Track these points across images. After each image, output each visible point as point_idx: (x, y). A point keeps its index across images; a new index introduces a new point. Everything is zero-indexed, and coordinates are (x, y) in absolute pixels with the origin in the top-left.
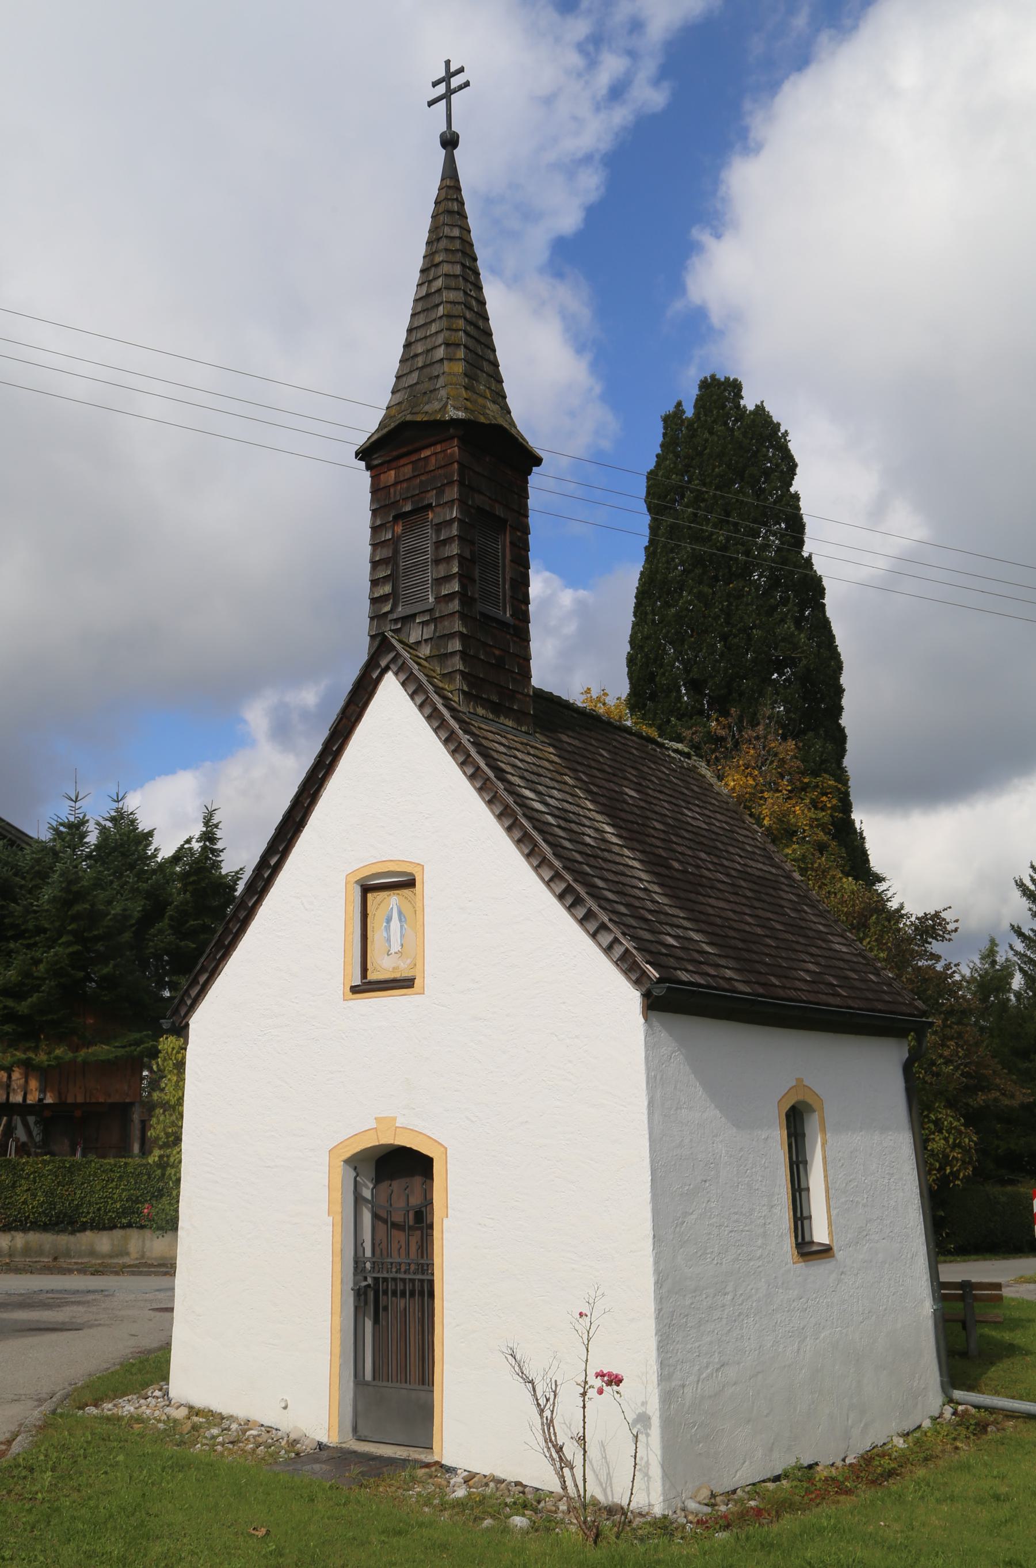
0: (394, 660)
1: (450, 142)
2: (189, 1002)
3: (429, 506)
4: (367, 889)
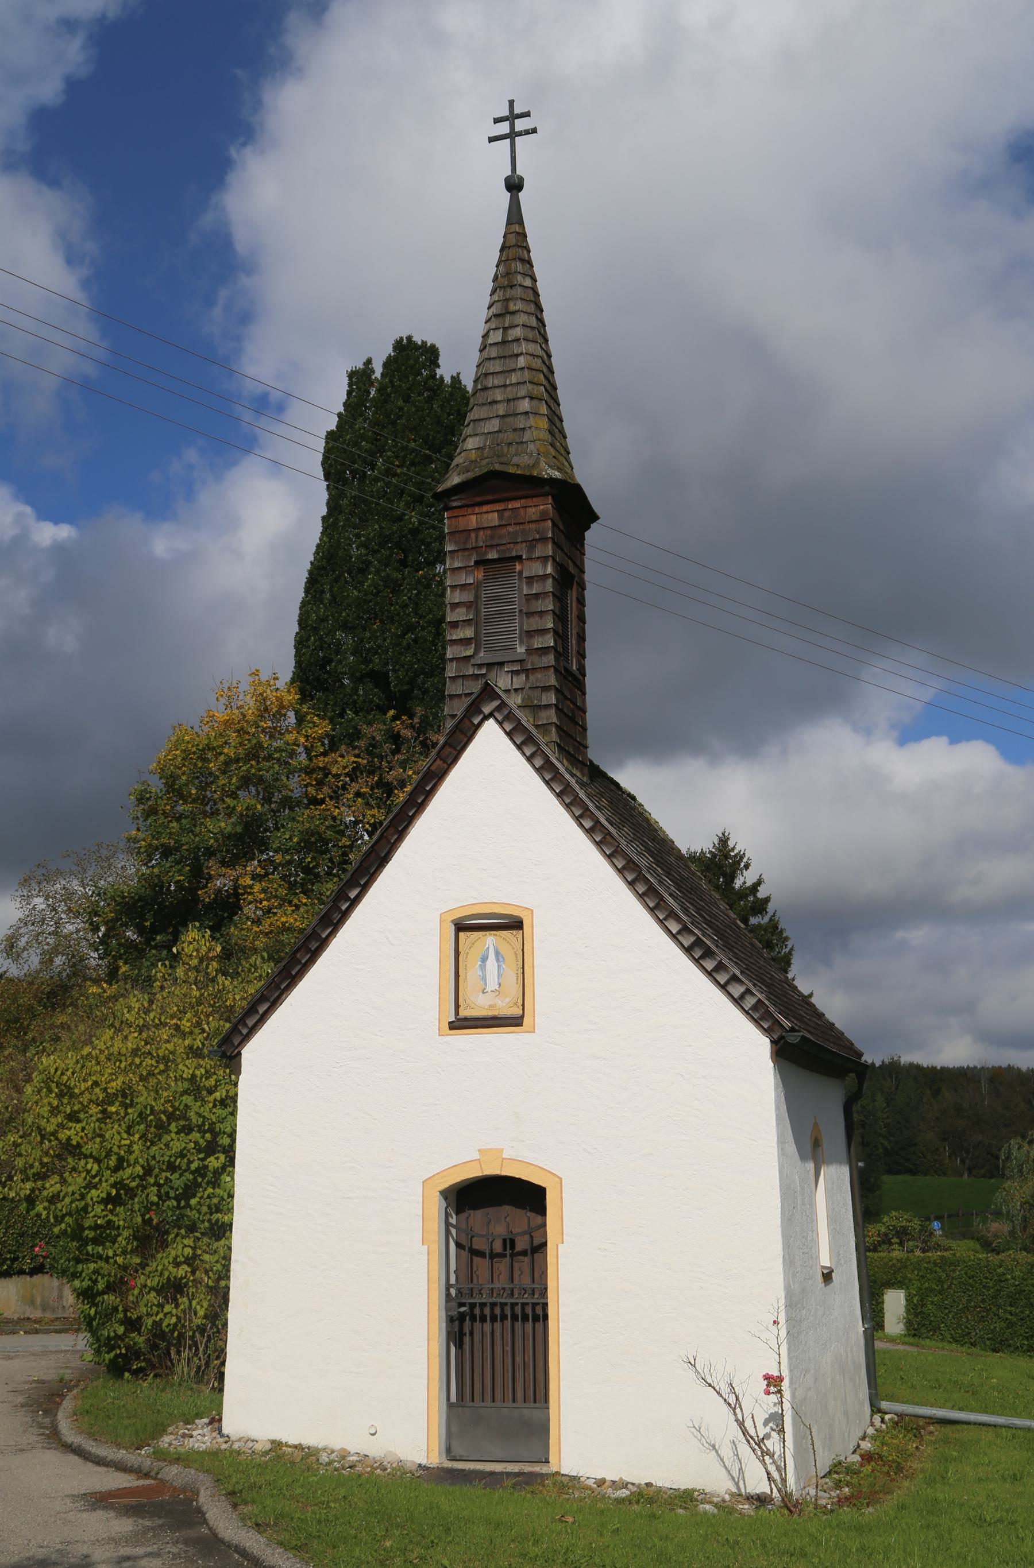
0: (498, 709)
1: (514, 185)
2: (245, 1031)
3: (519, 558)
4: (461, 927)
